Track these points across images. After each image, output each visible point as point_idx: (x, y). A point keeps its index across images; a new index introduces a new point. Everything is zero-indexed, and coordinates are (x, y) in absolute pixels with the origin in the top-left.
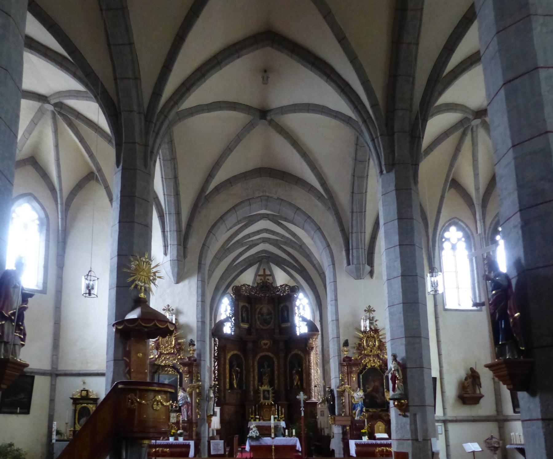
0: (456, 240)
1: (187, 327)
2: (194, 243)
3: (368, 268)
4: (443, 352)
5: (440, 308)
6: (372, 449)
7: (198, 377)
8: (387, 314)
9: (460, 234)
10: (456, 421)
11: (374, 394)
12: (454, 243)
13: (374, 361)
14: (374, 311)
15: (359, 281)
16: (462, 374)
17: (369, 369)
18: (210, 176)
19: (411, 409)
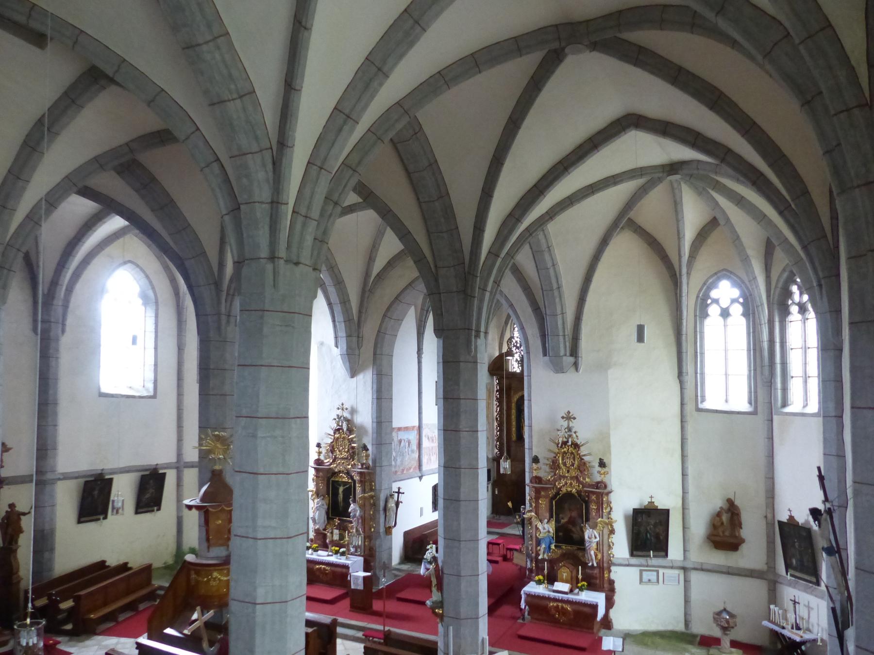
0: (729, 302)
1: (362, 429)
2: (369, 330)
3: (572, 359)
4: (690, 471)
5: (690, 407)
6: (544, 603)
7: (371, 485)
8: (462, 490)
9: (736, 293)
10: (702, 569)
11: (570, 526)
12: (724, 306)
13: (571, 484)
14: (574, 418)
15: (560, 376)
16: (718, 503)
17: (565, 495)
18: (371, 259)
19: (445, 619)
